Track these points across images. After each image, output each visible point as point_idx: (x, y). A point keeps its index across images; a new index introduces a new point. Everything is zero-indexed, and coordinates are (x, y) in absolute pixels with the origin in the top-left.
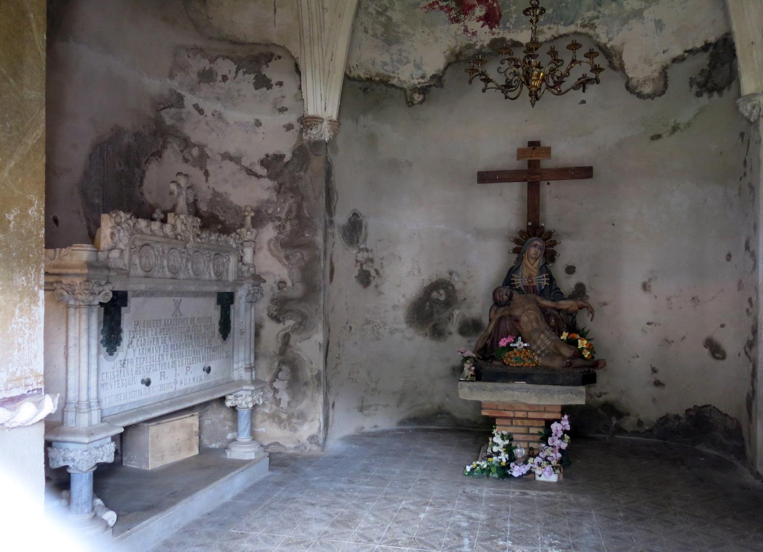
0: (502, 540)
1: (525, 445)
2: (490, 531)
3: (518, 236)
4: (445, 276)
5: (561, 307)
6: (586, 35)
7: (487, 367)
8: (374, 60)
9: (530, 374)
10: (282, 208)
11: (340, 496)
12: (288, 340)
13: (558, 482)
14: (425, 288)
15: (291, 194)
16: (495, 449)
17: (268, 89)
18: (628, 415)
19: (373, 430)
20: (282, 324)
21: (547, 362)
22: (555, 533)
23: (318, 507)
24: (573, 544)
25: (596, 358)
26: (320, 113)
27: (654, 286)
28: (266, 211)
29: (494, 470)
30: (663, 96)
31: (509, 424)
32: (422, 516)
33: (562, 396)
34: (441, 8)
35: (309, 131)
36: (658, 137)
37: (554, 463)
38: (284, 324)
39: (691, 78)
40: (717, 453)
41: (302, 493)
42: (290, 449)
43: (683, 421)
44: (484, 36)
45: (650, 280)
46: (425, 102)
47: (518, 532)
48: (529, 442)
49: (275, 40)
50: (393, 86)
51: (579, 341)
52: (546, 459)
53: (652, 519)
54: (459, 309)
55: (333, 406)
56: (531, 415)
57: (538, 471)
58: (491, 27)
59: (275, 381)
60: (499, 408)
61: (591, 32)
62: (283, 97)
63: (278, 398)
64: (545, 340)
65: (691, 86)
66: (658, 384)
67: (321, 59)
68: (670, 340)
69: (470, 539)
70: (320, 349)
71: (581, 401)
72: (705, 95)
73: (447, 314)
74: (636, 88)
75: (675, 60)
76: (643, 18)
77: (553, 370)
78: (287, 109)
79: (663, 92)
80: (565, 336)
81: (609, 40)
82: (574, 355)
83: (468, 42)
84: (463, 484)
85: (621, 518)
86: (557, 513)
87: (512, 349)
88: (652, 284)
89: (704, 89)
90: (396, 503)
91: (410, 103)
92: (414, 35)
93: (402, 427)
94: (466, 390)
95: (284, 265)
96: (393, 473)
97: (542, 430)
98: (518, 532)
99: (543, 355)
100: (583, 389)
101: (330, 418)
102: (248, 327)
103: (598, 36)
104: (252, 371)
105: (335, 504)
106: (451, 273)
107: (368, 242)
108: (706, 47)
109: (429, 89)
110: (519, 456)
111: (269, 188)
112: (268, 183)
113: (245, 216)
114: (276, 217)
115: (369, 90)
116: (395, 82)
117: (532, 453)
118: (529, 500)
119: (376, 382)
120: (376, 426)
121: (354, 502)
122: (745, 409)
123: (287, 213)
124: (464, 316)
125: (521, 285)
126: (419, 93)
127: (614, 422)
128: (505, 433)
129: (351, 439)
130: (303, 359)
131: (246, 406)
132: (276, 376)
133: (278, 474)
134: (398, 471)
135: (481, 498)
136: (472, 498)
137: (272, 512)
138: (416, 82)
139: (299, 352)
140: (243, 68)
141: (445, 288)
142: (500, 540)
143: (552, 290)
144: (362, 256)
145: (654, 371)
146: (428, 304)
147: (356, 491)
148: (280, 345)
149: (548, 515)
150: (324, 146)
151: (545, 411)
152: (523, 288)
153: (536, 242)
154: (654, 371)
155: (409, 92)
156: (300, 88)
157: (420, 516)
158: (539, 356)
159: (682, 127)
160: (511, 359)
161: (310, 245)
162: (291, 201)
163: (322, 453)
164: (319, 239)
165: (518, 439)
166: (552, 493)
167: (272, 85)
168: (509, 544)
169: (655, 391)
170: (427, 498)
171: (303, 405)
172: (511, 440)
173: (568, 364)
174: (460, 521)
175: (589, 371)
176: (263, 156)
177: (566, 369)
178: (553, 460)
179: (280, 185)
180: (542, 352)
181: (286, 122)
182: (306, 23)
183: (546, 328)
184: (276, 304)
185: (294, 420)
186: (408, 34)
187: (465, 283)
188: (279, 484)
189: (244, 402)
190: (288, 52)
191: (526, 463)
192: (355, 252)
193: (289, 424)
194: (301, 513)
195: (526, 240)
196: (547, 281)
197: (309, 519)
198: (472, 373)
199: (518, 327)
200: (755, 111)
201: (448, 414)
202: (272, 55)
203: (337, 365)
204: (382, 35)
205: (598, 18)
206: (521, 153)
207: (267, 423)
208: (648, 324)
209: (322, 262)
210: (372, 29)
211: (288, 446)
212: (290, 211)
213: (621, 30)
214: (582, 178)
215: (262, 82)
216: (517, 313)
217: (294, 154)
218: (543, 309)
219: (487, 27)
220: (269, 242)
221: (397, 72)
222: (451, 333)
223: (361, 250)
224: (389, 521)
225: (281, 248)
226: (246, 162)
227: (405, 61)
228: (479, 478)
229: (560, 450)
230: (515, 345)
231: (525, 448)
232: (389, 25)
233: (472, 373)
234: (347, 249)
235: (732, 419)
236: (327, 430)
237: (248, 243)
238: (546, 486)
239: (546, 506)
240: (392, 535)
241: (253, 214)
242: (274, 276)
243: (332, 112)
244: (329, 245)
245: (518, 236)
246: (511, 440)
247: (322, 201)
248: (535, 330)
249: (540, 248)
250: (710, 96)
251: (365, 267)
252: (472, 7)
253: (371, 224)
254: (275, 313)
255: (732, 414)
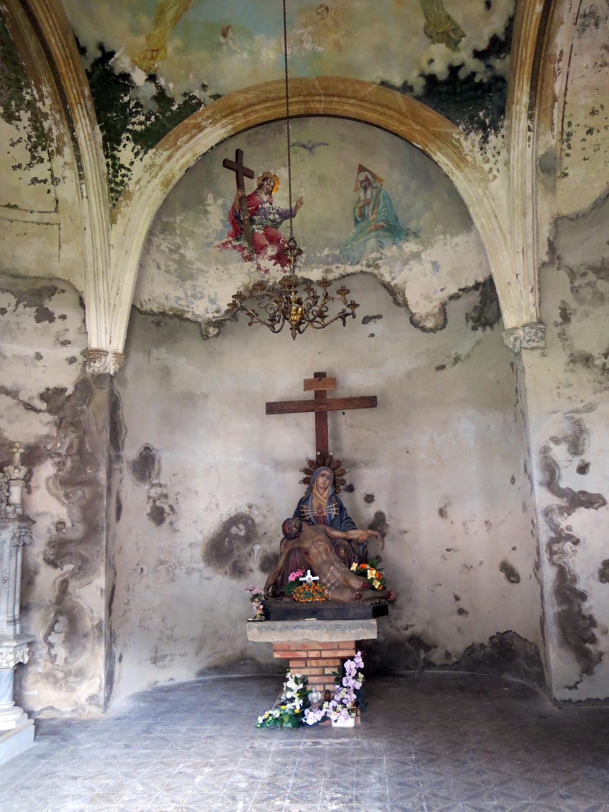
0: (280, 800)
1: (320, 688)
2: (270, 790)
3: (307, 466)
4: (245, 510)
5: (351, 537)
6: (371, 274)
7: (276, 605)
8: (164, 293)
9: (320, 609)
10: (63, 443)
11: (109, 764)
12: (67, 587)
13: (356, 727)
14: (224, 523)
15: (73, 429)
16: (289, 695)
17: (50, 322)
18: (436, 647)
19: (168, 684)
20: (60, 569)
21: (337, 596)
22: (339, 785)
23: (80, 781)
24: (356, 797)
25: (388, 589)
26: (104, 346)
27: (450, 511)
28: (45, 447)
29: (286, 719)
30: (443, 331)
31: (303, 665)
32: (198, 779)
33: (353, 632)
34: (235, 247)
35: (92, 364)
36: (442, 367)
37: (349, 705)
38: (62, 569)
39: (466, 314)
40: (520, 681)
41: (66, 765)
42: (66, 712)
43: (488, 650)
44: (276, 273)
45: (446, 506)
46: (221, 335)
47: (300, 788)
48: (324, 684)
49: (59, 274)
50: (188, 319)
51: (369, 571)
52: (341, 702)
53: (444, 759)
54: (260, 544)
55: (120, 660)
56: (325, 654)
57: (333, 716)
58: (283, 266)
59: (50, 634)
60: (291, 649)
61: (376, 272)
62: (67, 330)
63: (53, 654)
64: (335, 573)
65: (468, 321)
66: (461, 612)
67: (106, 293)
68: (469, 566)
69: (245, 803)
70: (102, 596)
71: (373, 635)
72: (480, 329)
73: (247, 550)
74: (419, 322)
75: (451, 298)
76: (421, 260)
77: (343, 603)
78: (69, 342)
79: (444, 327)
80: (354, 567)
81: (393, 279)
82: (363, 586)
83: (261, 279)
84: (253, 738)
85: (412, 761)
86: (346, 762)
87: (301, 583)
88: (448, 509)
89: (478, 323)
90: (172, 767)
91: (205, 337)
92: (208, 272)
93: (202, 678)
94: (255, 631)
95: (64, 504)
96: (178, 732)
97: (336, 670)
98: (300, 788)
99: (333, 588)
100: (374, 622)
101: (116, 674)
102: (12, 574)
103: (382, 275)
104: (15, 624)
105: (102, 774)
106: (250, 507)
107: (161, 477)
108: (477, 286)
109: (224, 322)
110: (315, 701)
111: (48, 423)
112: (48, 417)
113: (14, 453)
114: (56, 453)
115: (162, 324)
116: (189, 316)
117: (328, 696)
118: (320, 750)
119: (172, 629)
120: (172, 679)
121: (125, 770)
122: (539, 631)
123: (66, 450)
124: (264, 550)
125: (311, 516)
126: (214, 327)
127: (423, 656)
128: (299, 676)
129: (142, 696)
130: (82, 607)
131: (6, 666)
132: (52, 629)
133: (45, 744)
134: (184, 730)
135: (268, 753)
136: (258, 754)
137: (24, 792)
138: (211, 316)
139: (78, 600)
140: (23, 301)
141: (245, 523)
142: (278, 799)
143: (343, 519)
144: (154, 492)
145: (457, 599)
146: (227, 540)
147: (129, 757)
148: (57, 593)
149: (336, 765)
150: (108, 379)
151: (339, 649)
152: (313, 519)
153: (324, 472)
154: (457, 599)
155: (203, 326)
156: (84, 322)
157: (195, 780)
158: (329, 589)
159: (462, 358)
160: (300, 594)
161: (92, 482)
162: (73, 436)
163: (102, 715)
164: (102, 475)
165: (313, 682)
166: (346, 740)
167: (55, 318)
168: (287, 803)
169: (460, 619)
170: (208, 757)
171: (83, 660)
172: (306, 683)
173: (358, 597)
174: (239, 782)
175: (380, 603)
176: (42, 390)
177: (356, 602)
178: (348, 702)
179: (61, 420)
180: (333, 585)
181: (69, 355)
182: (90, 259)
183: (336, 560)
184: (53, 547)
185: (71, 679)
186: (202, 271)
187: (265, 517)
188: (42, 756)
189: (4, 661)
190: (72, 285)
191: (321, 708)
192: (147, 487)
193: (66, 684)
194: (58, 790)
195: (315, 469)
196: (336, 511)
197: (65, 797)
198: (261, 612)
199: (308, 560)
200: (517, 343)
201: (252, 659)
202: (56, 289)
203: (125, 612)
204: (176, 271)
205: (381, 259)
206: (308, 385)
207: (40, 685)
208: (448, 550)
209: (105, 500)
210: (166, 266)
211: (63, 710)
212: (71, 446)
213: (402, 270)
214: (367, 407)
215: (44, 315)
216: (306, 545)
217: (76, 387)
218: (333, 541)
219: (278, 265)
220: (48, 480)
221: (191, 306)
222: (251, 570)
223: (153, 486)
224: (158, 790)
225: (61, 485)
226: (23, 396)
227: (199, 296)
228: (272, 729)
229: (355, 691)
230: (304, 579)
231: (321, 692)
232: (182, 262)
233: (261, 612)
234: (136, 485)
235: (531, 643)
236: (111, 688)
237: (15, 482)
238: (343, 733)
239: (336, 755)
240: (158, 806)
241: (22, 451)
242: (52, 516)
243: (118, 345)
244: (115, 481)
245: (307, 466)
246: (306, 683)
247: (106, 436)
248: (324, 562)
249: (328, 478)
250: (484, 330)
251: (158, 503)
252: (263, 247)
253: (166, 461)
254: (52, 557)
255: (530, 639)
